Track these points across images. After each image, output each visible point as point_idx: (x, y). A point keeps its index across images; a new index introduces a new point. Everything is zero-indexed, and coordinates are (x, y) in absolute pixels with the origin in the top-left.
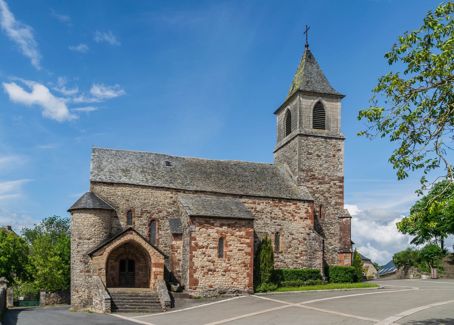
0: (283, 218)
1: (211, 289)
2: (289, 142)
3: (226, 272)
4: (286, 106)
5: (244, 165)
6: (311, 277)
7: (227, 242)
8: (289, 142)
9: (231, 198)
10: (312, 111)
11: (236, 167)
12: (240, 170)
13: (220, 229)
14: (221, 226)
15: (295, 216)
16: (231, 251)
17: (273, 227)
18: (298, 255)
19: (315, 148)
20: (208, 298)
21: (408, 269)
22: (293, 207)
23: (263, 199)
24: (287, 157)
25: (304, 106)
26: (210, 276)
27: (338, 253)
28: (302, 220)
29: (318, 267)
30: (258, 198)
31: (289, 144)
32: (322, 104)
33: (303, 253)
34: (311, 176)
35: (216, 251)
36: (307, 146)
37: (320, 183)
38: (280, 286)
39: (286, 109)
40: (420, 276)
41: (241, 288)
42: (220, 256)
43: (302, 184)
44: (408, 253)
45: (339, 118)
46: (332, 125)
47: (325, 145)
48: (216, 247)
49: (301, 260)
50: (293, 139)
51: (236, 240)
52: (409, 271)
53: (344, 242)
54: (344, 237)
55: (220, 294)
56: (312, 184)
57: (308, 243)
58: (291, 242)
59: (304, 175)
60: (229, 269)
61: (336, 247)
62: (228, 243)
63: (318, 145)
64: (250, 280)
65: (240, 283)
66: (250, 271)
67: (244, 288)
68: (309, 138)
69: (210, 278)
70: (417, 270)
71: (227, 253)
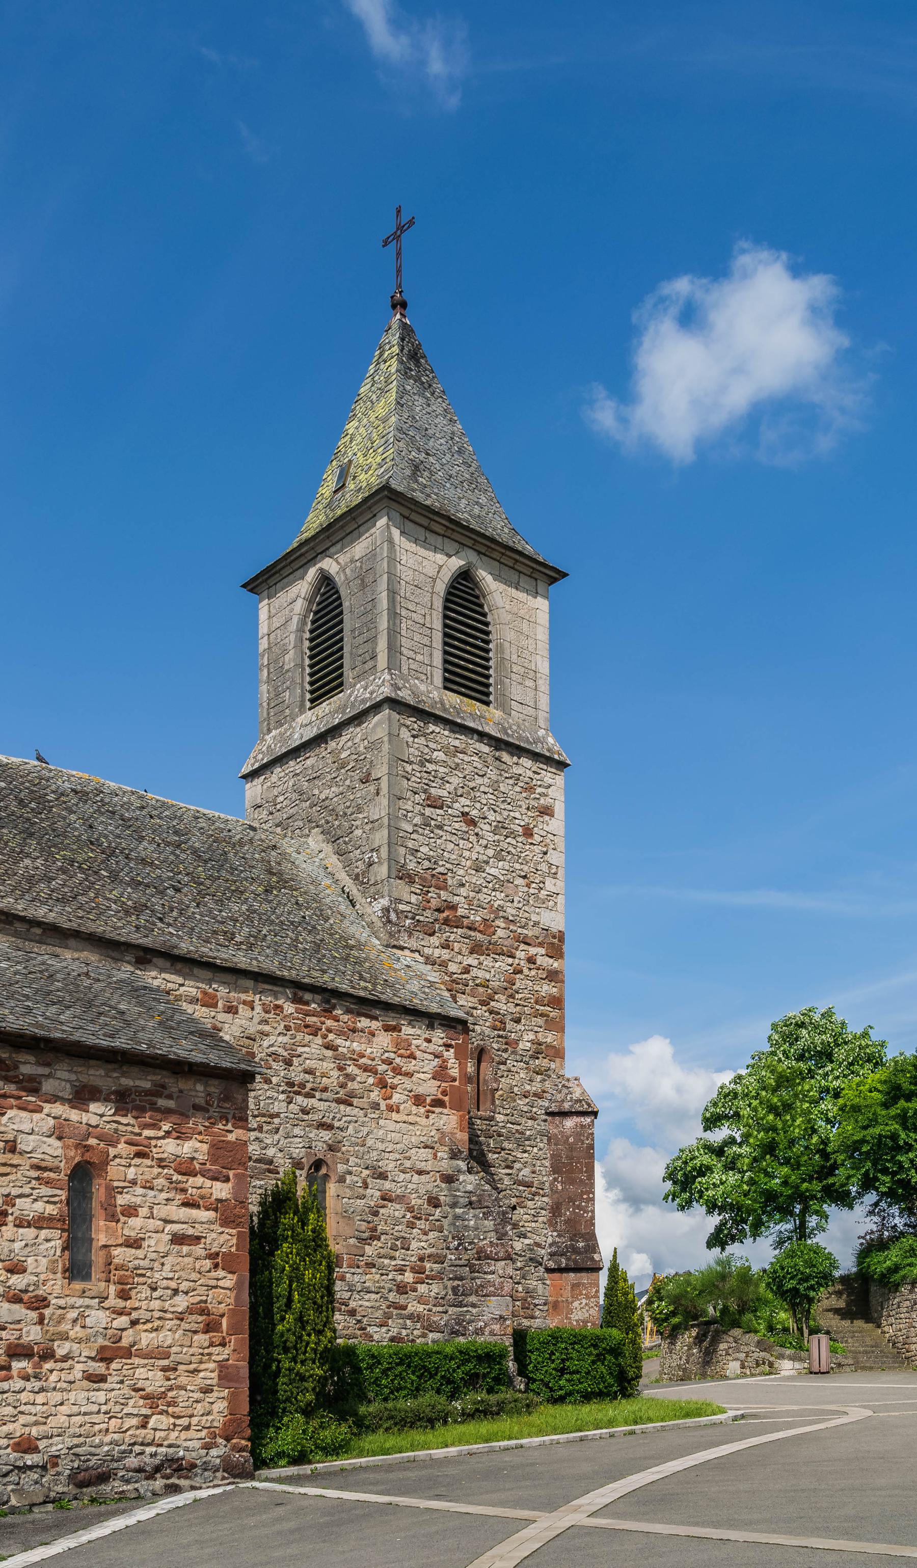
0: (342, 1093)
1: (29, 1460)
2: (334, 732)
3: (108, 1360)
4: (312, 561)
5: (127, 806)
6: (472, 1380)
7: (112, 1191)
8: (334, 732)
9: (92, 957)
10: (439, 604)
11: (89, 809)
12: (106, 827)
13: (74, 1115)
14: (82, 1096)
15: (394, 1087)
16: (134, 1243)
17: (297, 1131)
18: (409, 1277)
19: (455, 781)
20: (14, 1511)
21: (715, 1341)
22: (384, 1040)
23: (250, 983)
24: (324, 805)
25: (406, 575)
26: (18, 1384)
27: (549, 1270)
28: (422, 1110)
29: (492, 1333)
30: (229, 978)
31: (332, 744)
32: (476, 584)
33: (428, 1265)
34: (439, 910)
35: (52, 1242)
36: (422, 764)
37: (476, 949)
38: (362, 1426)
39: (312, 573)
40: (771, 1365)
41: (189, 1444)
42: (76, 1270)
43: (404, 940)
44: (723, 1277)
45: (544, 666)
46: (516, 692)
47: (492, 773)
48: (51, 1218)
49: (421, 1300)
50: (358, 718)
51: (161, 1181)
52: (723, 1346)
53: (567, 1222)
54: (571, 1200)
55: (81, 1485)
56: (446, 946)
57: (446, 1222)
58: (376, 1214)
59: (414, 899)
60: (125, 1343)
61: (538, 1245)
62: (121, 1200)
63: (469, 769)
64: (232, 1400)
65: (184, 1422)
66: (233, 1352)
67: (207, 1447)
68: (432, 727)
69: (24, 1397)
70: (759, 1343)
71: (116, 1252)
